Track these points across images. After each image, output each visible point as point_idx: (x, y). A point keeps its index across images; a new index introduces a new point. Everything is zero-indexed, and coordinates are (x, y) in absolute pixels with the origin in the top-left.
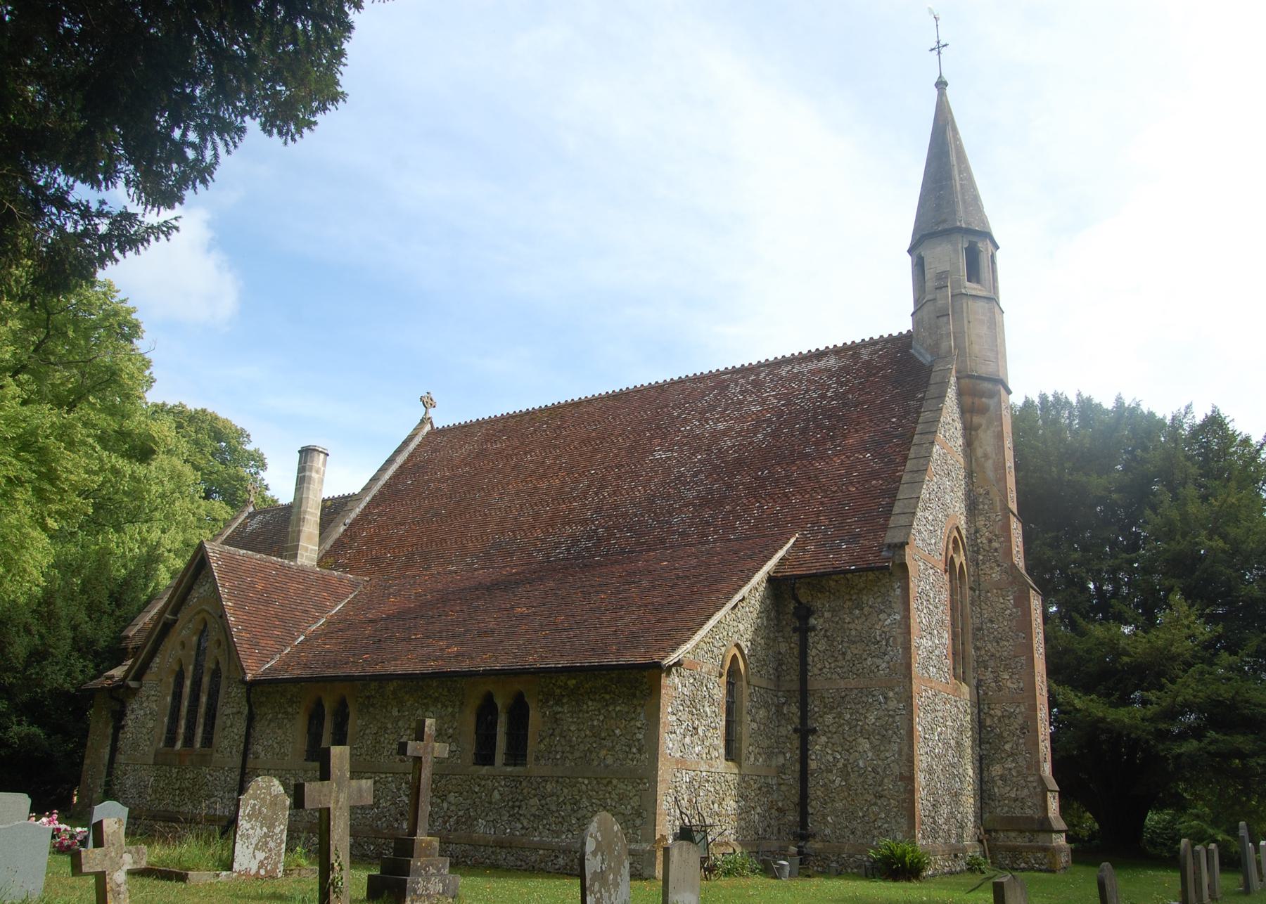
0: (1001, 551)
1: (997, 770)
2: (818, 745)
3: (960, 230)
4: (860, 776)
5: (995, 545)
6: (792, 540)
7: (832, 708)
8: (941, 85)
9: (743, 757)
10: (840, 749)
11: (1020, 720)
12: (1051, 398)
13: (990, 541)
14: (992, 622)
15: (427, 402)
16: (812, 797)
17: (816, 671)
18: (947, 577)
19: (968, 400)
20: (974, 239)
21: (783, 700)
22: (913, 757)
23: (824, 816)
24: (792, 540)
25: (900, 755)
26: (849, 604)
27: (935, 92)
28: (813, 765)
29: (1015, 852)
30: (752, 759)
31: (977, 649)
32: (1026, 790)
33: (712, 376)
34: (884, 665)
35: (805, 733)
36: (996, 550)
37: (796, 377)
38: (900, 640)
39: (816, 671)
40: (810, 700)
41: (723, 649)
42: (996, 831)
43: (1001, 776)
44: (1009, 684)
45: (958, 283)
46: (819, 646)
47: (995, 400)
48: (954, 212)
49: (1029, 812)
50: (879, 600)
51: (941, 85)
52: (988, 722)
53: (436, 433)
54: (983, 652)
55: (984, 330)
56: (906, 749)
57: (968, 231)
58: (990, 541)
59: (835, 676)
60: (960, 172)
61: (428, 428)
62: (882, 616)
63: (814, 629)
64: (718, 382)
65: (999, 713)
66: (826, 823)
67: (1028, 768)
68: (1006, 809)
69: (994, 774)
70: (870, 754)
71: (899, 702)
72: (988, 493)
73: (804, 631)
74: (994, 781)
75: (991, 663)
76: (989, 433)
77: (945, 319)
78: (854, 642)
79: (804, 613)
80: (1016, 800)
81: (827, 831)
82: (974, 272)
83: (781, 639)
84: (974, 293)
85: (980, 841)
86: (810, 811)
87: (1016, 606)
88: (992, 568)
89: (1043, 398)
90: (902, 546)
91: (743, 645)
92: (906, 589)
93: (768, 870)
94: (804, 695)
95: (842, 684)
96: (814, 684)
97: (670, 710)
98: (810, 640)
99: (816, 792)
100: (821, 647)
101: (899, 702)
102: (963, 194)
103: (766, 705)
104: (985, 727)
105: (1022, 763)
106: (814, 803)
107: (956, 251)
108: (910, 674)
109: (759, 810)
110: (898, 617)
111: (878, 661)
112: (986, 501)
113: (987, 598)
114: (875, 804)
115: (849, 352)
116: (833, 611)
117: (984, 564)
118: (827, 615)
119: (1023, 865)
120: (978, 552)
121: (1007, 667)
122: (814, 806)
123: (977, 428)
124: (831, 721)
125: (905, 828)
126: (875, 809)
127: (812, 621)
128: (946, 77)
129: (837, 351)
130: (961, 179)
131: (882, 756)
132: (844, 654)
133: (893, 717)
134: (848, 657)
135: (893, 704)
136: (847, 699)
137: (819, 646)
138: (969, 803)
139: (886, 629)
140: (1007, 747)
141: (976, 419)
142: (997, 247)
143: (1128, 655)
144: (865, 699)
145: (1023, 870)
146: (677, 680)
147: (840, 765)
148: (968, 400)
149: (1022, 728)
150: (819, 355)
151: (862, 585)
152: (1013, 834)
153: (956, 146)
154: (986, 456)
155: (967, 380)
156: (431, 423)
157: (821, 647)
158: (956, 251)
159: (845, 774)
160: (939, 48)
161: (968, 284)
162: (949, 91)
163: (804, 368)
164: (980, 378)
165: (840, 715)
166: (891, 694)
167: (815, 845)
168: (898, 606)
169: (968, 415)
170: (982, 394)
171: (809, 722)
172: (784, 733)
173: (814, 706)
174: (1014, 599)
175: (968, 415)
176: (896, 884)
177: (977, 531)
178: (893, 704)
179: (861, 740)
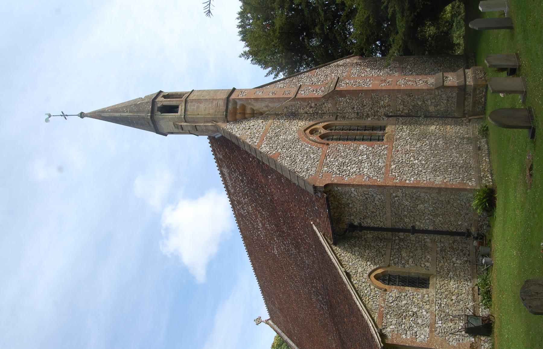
0: (316, 103)
1: (432, 109)
2: (419, 225)
3: (152, 117)
4: (437, 210)
5: (313, 105)
6: (315, 228)
7: (401, 218)
8: (82, 115)
9: (427, 272)
10: (423, 217)
11: (405, 97)
12: (240, 29)
13: (311, 107)
14: (353, 108)
15: (258, 321)
16: (448, 229)
17: (382, 224)
18: (332, 144)
19: (239, 116)
20: (156, 109)
21: (397, 238)
22: (428, 188)
23: (458, 225)
24: (315, 228)
25: (427, 193)
26: (346, 209)
27: (85, 118)
28: (431, 228)
29: (475, 103)
30: (428, 264)
31: (368, 116)
32: (443, 96)
33: (238, 222)
34: (379, 196)
35: (414, 230)
36: (316, 105)
37: (234, 187)
38: (365, 189)
39: (382, 224)
40: (397, 227)
41: (372, 287)
42: (464, 110)
43: (435, 107)
44: (386, 101)
45: (179, 118)
46: (369, 222)
47: (237, 101)
48: (143, 118)
49: (454, 95)
50: (344, 196)
51: (82, 115)
52: (406, 111)
53: (272, 318)
54: (369, 113)
55: (202, 106)
56: (423, 190)
57: (152, 112)
58: (311, 107)
59: (385, 217)
60: (124, 112)
61: (270, 322)
62: (353, 195)
63: (360, 224)
64: (240, 217)
65: (402, 106)
66: (461, 225)
67: (431, 94)
68: (452, 105)
69: (434, 110)
70: (426, 205)
71: (398, 191)
72: (286, 107)
73: (361, 228)
74: (437, 110)
75: (376, 109)
76: (255, 104)
77: (198, 127)
78: (367, 208)
79: (352, 227)
80: (448, 100)
81: (466, 224)
82: (173, 109)
83: (366, 237)
84: (183, 110)
85: (470, 120)
86: (455, 230)
87: (345, 97)
88: (325, 107)
89: (239, 27)
90: (315, 187)
91: (369, 270)
92: (338, 185)
93: (489, 267)
94: (394, 230)
95: (389, 214)
96: (389, 225)
97: (404, 336)
98: (366, 225)
99: (445, 228)
100: (369, 221)
101: (398, 191)
102: (134, 112)
103: (400, 250)
104: (409, 113)
105: (428, 97)
106: (451, 229)
107: (163, 119)
108: (383, 186)
109: (454, 259)
110: (353, 189)
111: (376, 199)
112: (290, 108)
113: (341, 110)
114: (453, 204)
115: (219, 161)
116: (350, 215)
117: (323, 110)
118: (352, 217)
119: (483, 100)
120: (317, 113)
121: (378, 102)
122: (452, 229)
123: (253, 110)
124: (408, 219)
125: (467, 193)
126: (455, 205)
127: (356, 224)
128: (79, 112)
129: (220, 166)
130: (127, 112)
131: (427, 200)
132: (373, 212)
133: (406, 194)
134: (375, 211)
135: (399, 194)
136: (397, 213)
137: (369, 222)
138: (451, 130)
139: (360, 195)
140: (420, 103)
141: (248, 111)
142: (161, 92)
143: (368, 18)
144: (397, 206)
145: (486, 100)
146: (389, 329)
147: (431, 217)
148: (239, 116)
149: (410, 96)
150: (222, 173)
151: (337, 203)
152: (466, 103)
153: (111, 112)
154: (267, 106)
155: (228, 117)
156: (268, 320)
157: (369, 221)
158: (163, 119)
159: (436, 216)
160: (64, 116)
161: (179, 114)
162: (86, 112)
163: (229, 184)
164: (227, 110)
165: (405, 216)
166: (394, 195)
167: (473, 230)
168: (347, 189)
169: (246, 116)
170: (235, 109)
171: (408, 228)
172: (414, 238)
173: (401, 226)
174: (341, 97)
175: (246, 116)
176: (497, 205)
177: (307, 113)
178: (399, 194)
179: (418, 208)
